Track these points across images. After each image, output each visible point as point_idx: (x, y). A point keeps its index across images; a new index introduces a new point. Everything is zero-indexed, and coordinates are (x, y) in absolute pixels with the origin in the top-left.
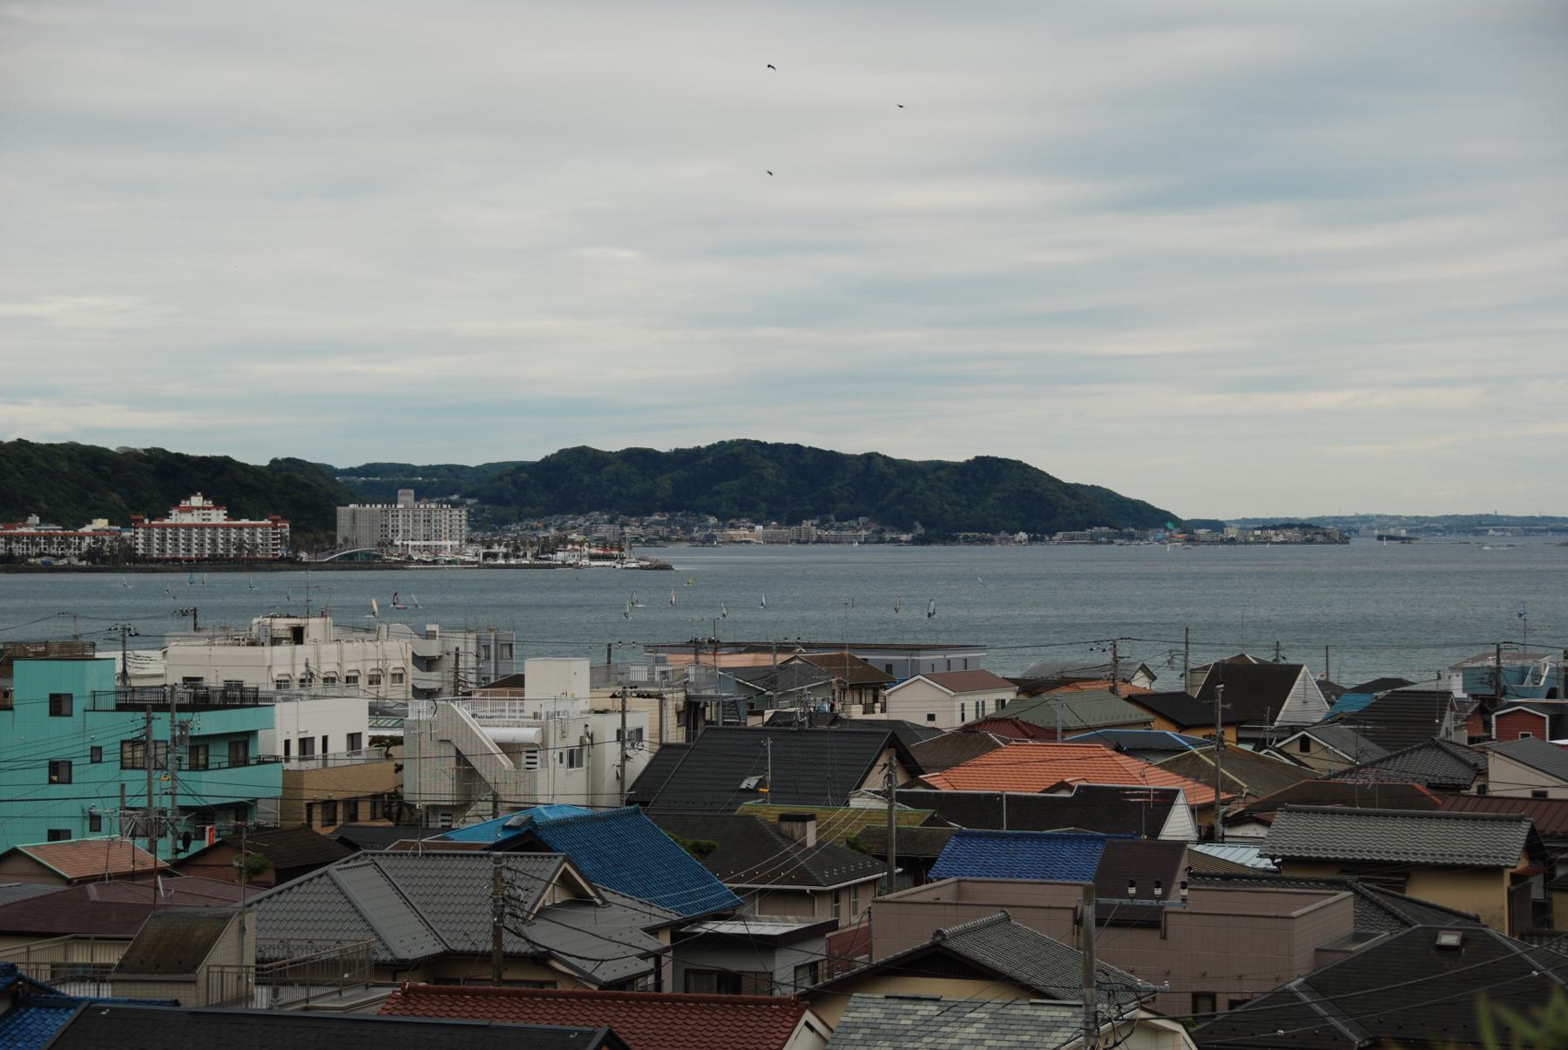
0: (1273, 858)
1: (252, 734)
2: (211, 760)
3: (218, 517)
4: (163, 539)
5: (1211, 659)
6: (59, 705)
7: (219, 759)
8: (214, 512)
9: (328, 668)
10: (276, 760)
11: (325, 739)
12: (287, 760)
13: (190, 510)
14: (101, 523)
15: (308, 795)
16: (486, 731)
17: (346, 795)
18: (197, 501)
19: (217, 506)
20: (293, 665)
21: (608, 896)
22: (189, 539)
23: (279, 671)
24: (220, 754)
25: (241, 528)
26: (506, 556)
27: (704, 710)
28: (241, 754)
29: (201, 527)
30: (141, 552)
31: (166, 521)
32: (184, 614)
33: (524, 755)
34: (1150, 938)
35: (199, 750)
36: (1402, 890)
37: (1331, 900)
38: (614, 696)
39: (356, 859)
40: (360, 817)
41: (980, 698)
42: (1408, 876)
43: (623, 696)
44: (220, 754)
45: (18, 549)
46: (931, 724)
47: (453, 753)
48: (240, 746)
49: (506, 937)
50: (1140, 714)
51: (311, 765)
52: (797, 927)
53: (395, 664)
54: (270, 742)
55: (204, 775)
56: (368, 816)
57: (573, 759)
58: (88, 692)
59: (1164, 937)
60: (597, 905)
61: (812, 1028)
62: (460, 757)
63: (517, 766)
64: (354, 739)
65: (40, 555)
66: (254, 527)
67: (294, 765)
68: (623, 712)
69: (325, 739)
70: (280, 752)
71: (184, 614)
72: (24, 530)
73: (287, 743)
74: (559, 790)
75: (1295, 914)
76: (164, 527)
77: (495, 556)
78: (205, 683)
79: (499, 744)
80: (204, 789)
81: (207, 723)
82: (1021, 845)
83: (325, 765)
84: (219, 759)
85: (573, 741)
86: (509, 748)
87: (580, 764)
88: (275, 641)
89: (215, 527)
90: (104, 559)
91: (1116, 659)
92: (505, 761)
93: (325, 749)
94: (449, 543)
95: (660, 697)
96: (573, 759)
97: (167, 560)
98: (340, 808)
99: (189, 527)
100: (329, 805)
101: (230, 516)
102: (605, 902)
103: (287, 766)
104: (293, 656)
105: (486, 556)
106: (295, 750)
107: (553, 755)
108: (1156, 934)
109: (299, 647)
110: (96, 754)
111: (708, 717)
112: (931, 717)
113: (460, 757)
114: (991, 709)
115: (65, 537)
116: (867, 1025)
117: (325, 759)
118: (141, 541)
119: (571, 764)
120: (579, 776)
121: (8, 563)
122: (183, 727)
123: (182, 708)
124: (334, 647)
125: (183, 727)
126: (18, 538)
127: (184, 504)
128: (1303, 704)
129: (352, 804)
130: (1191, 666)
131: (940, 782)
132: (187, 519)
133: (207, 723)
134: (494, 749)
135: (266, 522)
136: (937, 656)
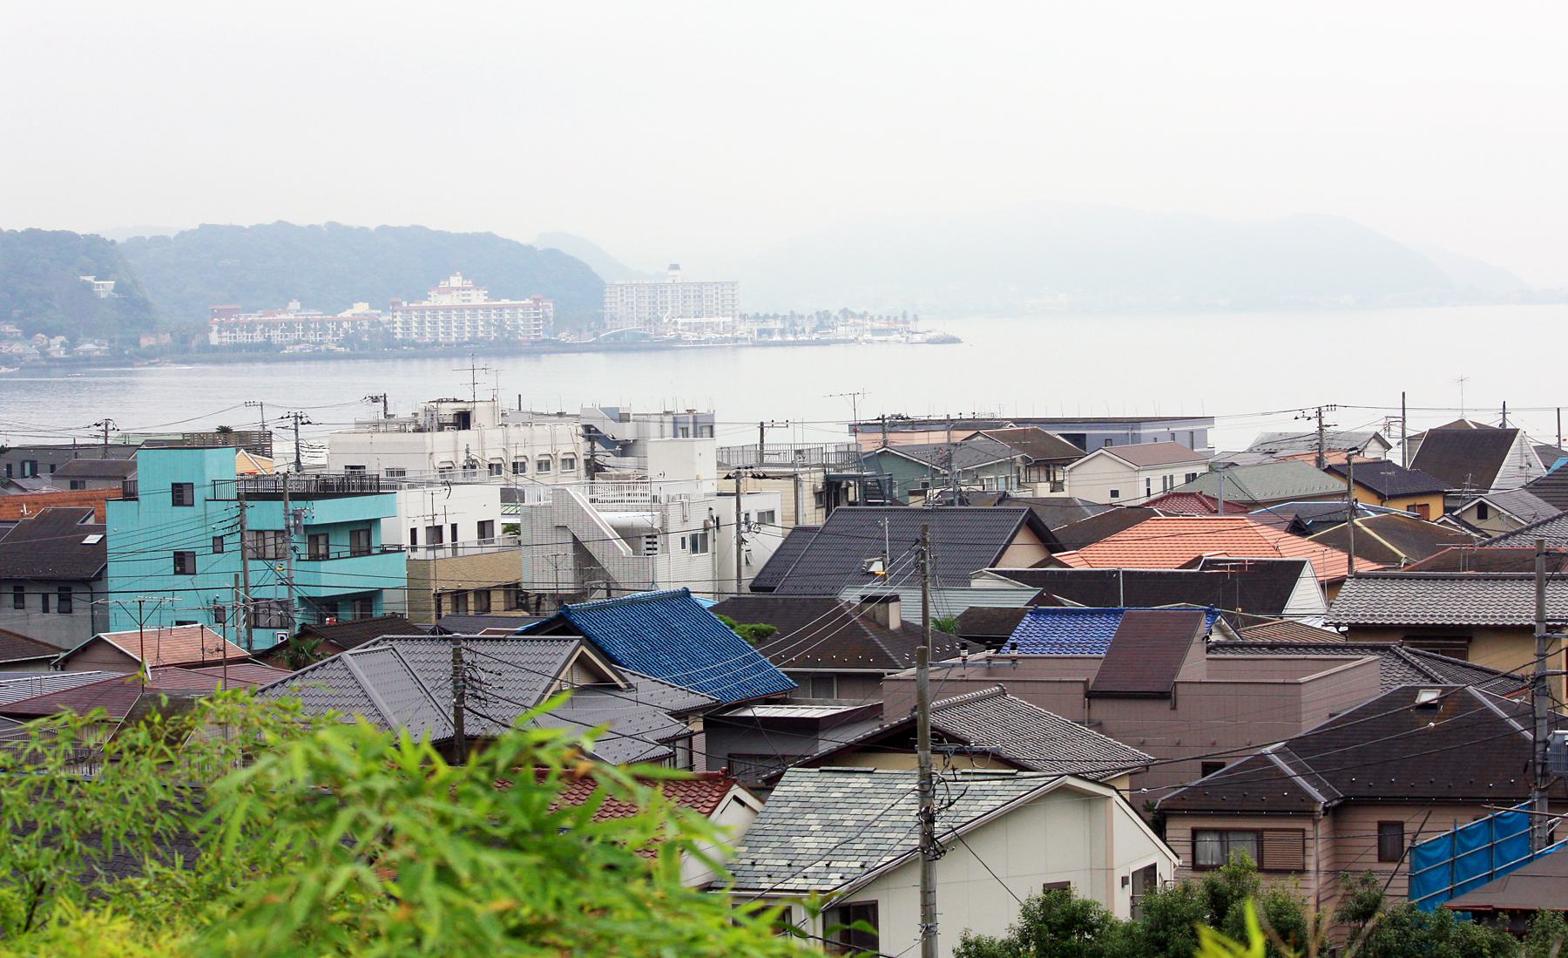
0: (1337, 626)
1: (374, 522)
2: (332, 549)
3: (478, 298)
4: (422, 323)
5: (1425, 428)
6: (181, 494)
7: (339, 549)
8: (474, 293)
9: (493, 454)
10: (400, 549)
11: (454, 527)
12: (414, 549)
13: (449, 290)
14: (361, 308)
15: (435, 587)
16: (603, 515)
17: (454, 586)
18: (456, 281)
19: (477, 286)
20: (456, 451)
21: (633, 680)
22: (448, 321)
23: (441, 458)
24: (341, 543)
25: (501, 308)
26: (782, 332)
27: (846, 490)
28: (364, 543)
29: (461, 309)
30: (399, 336)
31: (425, 303)
32: (375, 400)
33: (644, 540)
34: (1159, 710)
35: (318, 536)
36: (1465, 657)
37: (1351, 665)
38: (728, 477)
39: (375, 644)
40: (493, 606)
41: (1168, 473)
42: (1470, 640)
43: (738, 476)
44: (341, 543)
45: (276, 336)
46: (1115, 500)
47: (570, 539)
48: (361, 535)
49: (468, 719)
50: (1338, 485)
51: (440, 553)
52: (844, 709)
53: (565, 449)
54: (393, 531)
55: (324, 565)
56: (502, 606)
57: (697, 543)
58: (208, 481)
59: (1174, 708)
60: (618, 688)
61: (742, 803)
62: (577, 544)
63: (636, 551)
64: (484, 528)
65: (298, 342)
66: (515, 308)
67: (421, 554)
68: (737, 494)
69: (454, 527)
70: (407, 542)
71: (375, 400)
72: (283, 317)
73: (414, 531)
74: (677, 570)
75: (1302, 680)
76: (423, 310)
77: (770, 332)
78: (368, 471)
79: (617, 529)
80: (324, 580)
81: (325, 512)
82: (1096, 621)
83: (455, 554)
84: (339, 549)
85: (696, 524)
86: (628, 534)
87: (705, 549)
88: (441, 428)
89: (475, 309)
90: (363, 346)
91: (1321, 427)
92: (623, 548)
93: (454, 538)
94: (722, 319)
95: (794, 476)
96: (697, 543)
97: (427, 345)
98: (471, 598)
99: (448, 309)
100: (459, 596)
101: (492, 296)
102: (630, 686)
103: (414, 556)
104: (456, 443)
105: (761, 332)
106: (422, 539)
107: (674, 540)
108: (1166, 705)
109: (462, 433)
110: (218, 544)
111: (851, 498)
112: (1115, 494)
113: (577, 544)
114: (1179, 480)
115: (322, 322)
116: (798, 799)
117: (455, 547)
118: (399, 325)
119: (694, 549)
120: (703, 561)
121: (7, 361)
122: (297, 516)
123: (295, 497)
124: (499, 432)
125: (297, 516)
126: (274, 326)
127: (443, 284)
128: (1512, 473)
129: (484, 594)
130: (1409, 433)
131: (1075, 561)
132: (446, 300)
133: (325, 512)
134: (611, 534)
135: (527, 301)
136: (1161, 429)
